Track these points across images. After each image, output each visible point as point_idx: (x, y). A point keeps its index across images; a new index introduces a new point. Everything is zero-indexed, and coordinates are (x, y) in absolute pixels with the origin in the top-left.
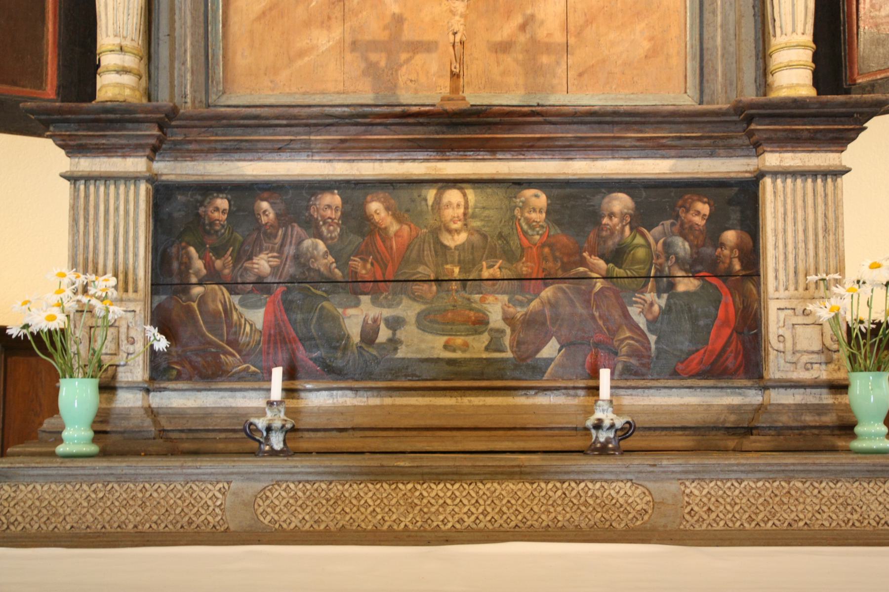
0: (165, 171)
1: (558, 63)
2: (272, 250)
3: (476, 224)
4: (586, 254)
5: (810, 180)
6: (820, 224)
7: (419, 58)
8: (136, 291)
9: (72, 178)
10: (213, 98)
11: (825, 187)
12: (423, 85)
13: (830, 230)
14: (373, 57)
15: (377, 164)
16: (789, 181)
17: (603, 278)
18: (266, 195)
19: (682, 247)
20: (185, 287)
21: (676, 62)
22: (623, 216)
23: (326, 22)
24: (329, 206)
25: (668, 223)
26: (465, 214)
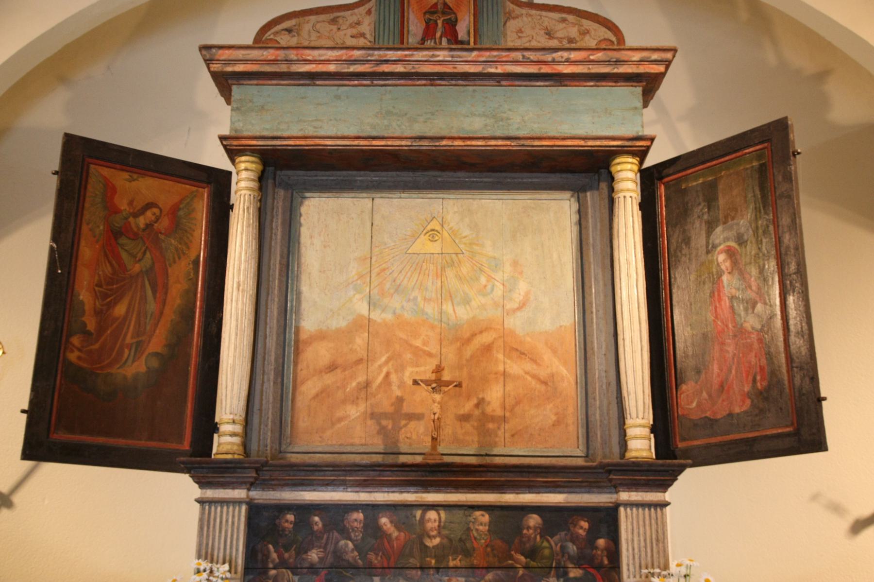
0: (257, 497)
1: (499, 428)
2: (320, 547)
3: (445, 532)
4: (513, 553)
5: (647, 509)
6: (654, 536)
7: (413, 424)
8: (236, 573)
9: (201, 501)
10: (284, 447)
11: (656, 513)
12: (415, 441)
13: (660, 539)
14: (384, 422)
15: (386, 494)
16: (634, 509)
17: (524, 568)
18: (317, 512)
19: (572, 548)
20: (266, 570)
21: (572, 428)
22: (535, 529)
23: (355, 401)
24: (356, 520)
25: (563, 533)
26: (439, 526)
